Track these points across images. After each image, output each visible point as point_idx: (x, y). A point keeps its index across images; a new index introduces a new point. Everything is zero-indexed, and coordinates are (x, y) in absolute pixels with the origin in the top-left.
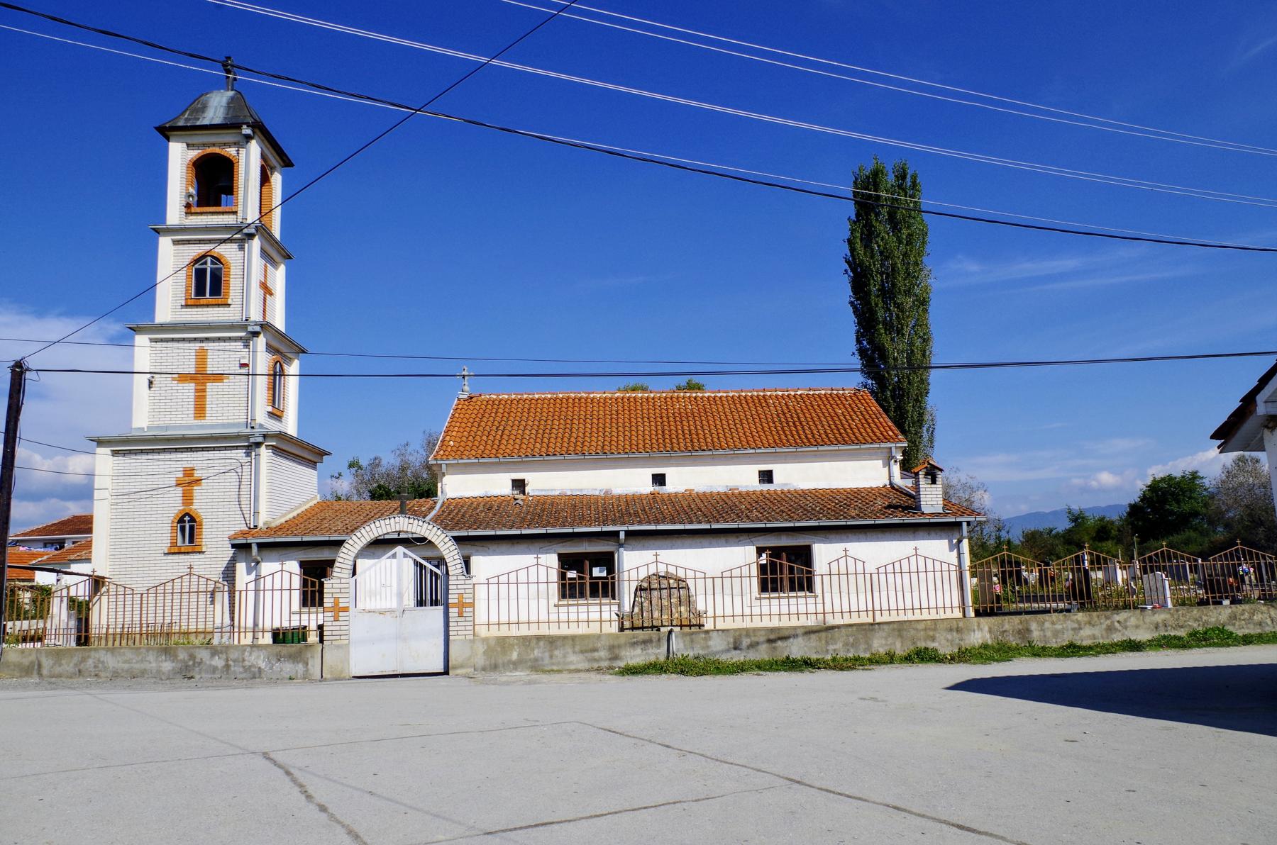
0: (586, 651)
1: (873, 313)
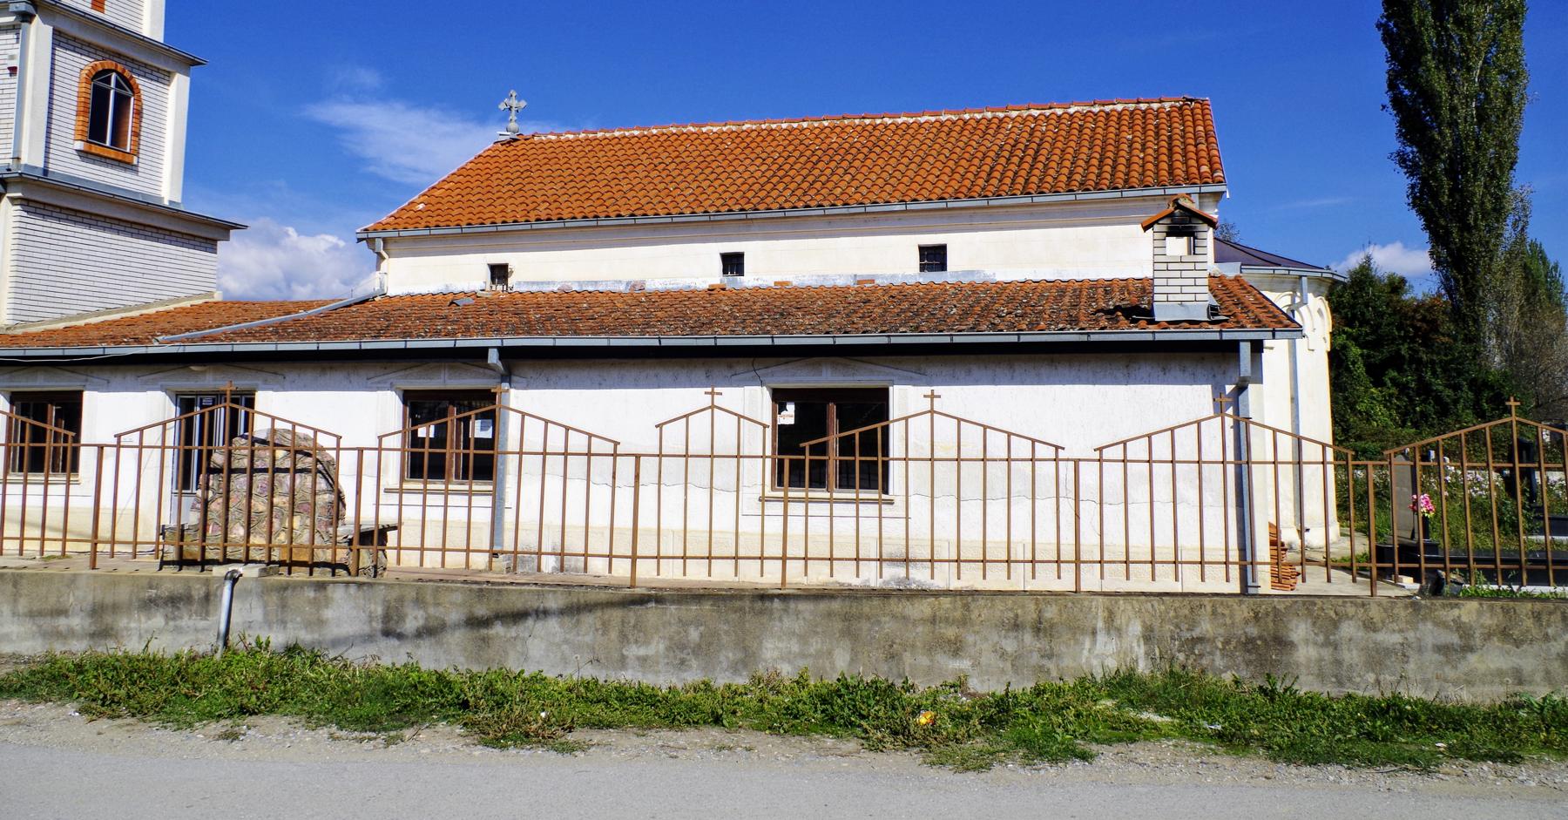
0: (41, 614)
1: (1415, 35)
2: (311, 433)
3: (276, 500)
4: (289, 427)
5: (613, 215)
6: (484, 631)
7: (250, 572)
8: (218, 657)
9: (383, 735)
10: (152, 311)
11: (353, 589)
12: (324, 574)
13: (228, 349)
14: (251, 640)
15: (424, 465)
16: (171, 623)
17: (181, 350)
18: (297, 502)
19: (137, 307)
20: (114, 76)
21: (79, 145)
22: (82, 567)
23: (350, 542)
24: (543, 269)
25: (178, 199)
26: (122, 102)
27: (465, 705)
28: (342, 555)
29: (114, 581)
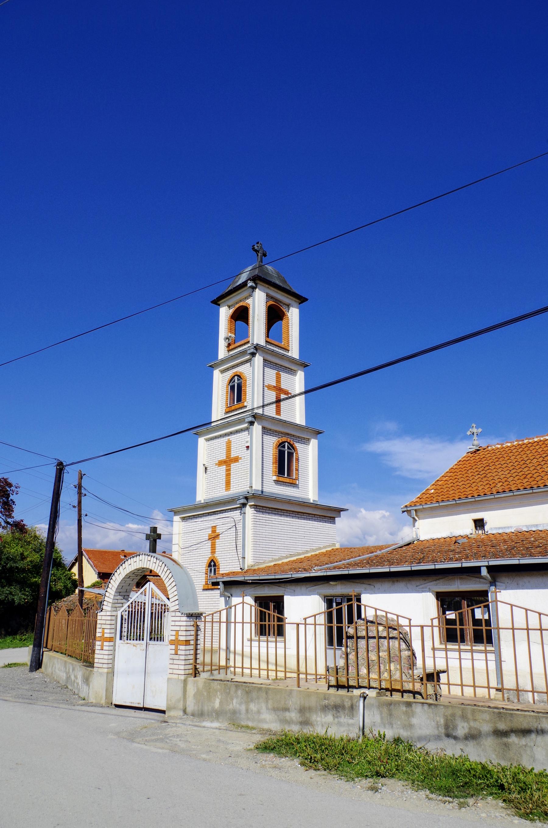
2: (395, 617)
3: (380, 654)
4: (384, 614)
5: (542, 486)
6: (505, 740)
7: (372, 694)
8: (360, 740)
9: (456, 801)
10: (309, 555)
11: (426, 707)
12: (409, 697)
13: (346, 572)
14: (376, 733)
15: (452, 635)
16: (336, 720)
17: (325, 574)
18: (392, 655)
19: (303, 553)
20: (286, 444)
21: (275, 478)
22: (292, 684)
23: (422, 679)
24: (504, 520)
25: (317, 499)
26: (290, 455)
27: (502, 787)
28: (418, 687)
29: (308, 694)
